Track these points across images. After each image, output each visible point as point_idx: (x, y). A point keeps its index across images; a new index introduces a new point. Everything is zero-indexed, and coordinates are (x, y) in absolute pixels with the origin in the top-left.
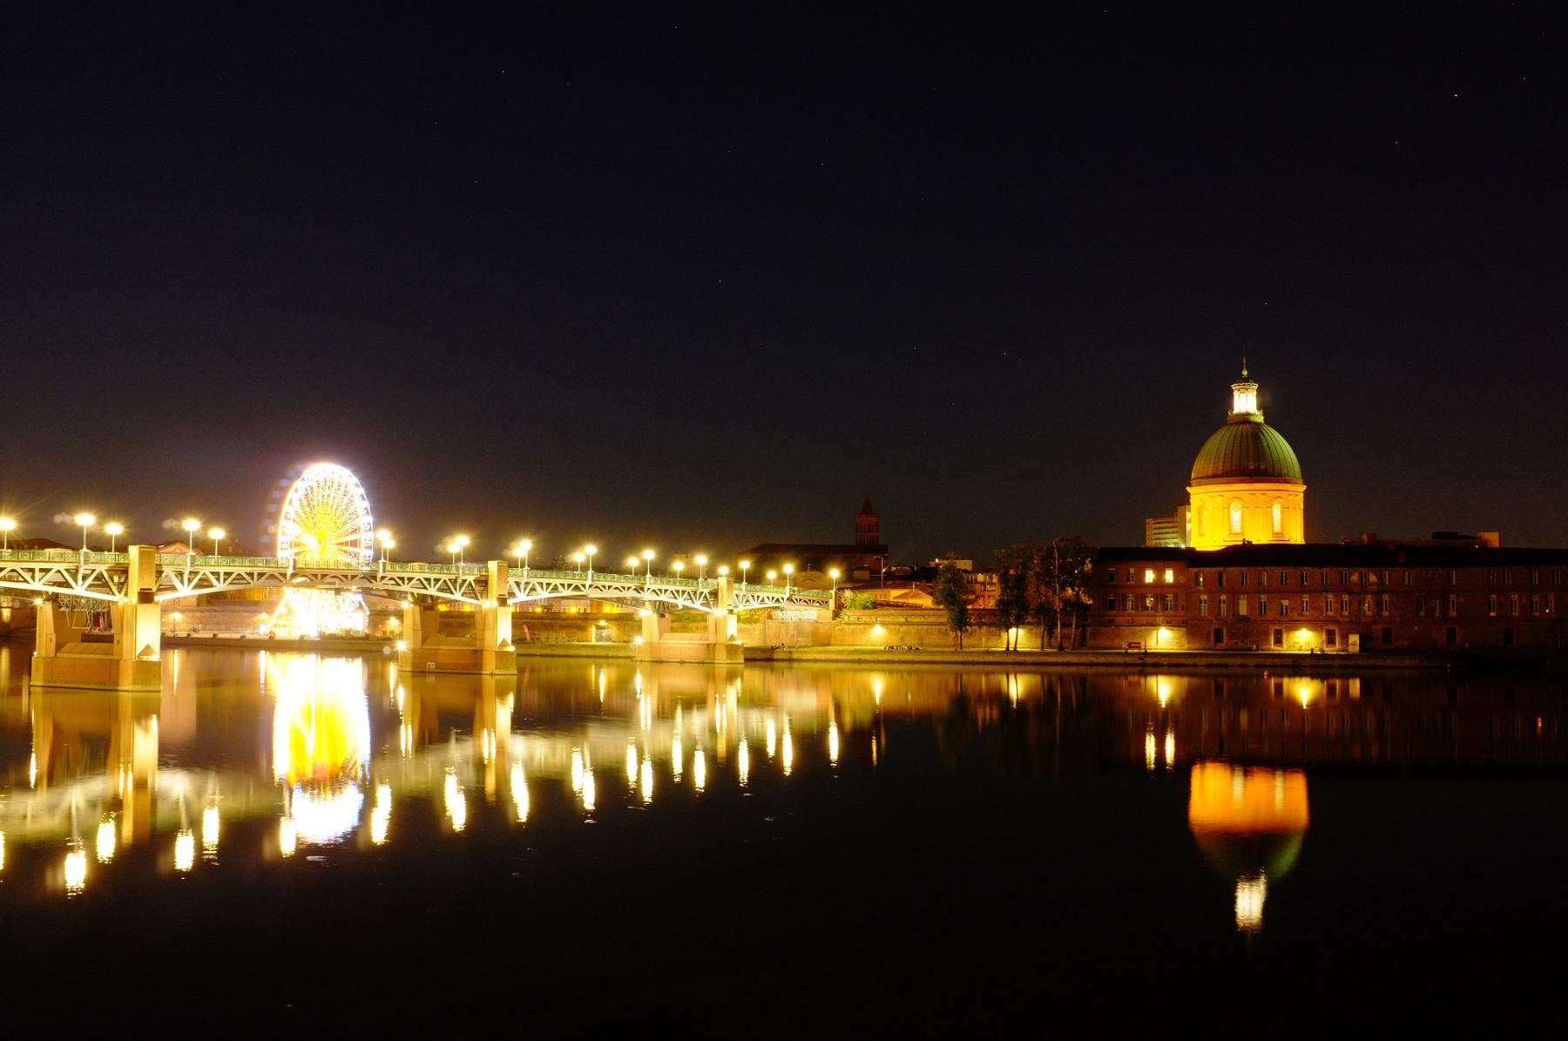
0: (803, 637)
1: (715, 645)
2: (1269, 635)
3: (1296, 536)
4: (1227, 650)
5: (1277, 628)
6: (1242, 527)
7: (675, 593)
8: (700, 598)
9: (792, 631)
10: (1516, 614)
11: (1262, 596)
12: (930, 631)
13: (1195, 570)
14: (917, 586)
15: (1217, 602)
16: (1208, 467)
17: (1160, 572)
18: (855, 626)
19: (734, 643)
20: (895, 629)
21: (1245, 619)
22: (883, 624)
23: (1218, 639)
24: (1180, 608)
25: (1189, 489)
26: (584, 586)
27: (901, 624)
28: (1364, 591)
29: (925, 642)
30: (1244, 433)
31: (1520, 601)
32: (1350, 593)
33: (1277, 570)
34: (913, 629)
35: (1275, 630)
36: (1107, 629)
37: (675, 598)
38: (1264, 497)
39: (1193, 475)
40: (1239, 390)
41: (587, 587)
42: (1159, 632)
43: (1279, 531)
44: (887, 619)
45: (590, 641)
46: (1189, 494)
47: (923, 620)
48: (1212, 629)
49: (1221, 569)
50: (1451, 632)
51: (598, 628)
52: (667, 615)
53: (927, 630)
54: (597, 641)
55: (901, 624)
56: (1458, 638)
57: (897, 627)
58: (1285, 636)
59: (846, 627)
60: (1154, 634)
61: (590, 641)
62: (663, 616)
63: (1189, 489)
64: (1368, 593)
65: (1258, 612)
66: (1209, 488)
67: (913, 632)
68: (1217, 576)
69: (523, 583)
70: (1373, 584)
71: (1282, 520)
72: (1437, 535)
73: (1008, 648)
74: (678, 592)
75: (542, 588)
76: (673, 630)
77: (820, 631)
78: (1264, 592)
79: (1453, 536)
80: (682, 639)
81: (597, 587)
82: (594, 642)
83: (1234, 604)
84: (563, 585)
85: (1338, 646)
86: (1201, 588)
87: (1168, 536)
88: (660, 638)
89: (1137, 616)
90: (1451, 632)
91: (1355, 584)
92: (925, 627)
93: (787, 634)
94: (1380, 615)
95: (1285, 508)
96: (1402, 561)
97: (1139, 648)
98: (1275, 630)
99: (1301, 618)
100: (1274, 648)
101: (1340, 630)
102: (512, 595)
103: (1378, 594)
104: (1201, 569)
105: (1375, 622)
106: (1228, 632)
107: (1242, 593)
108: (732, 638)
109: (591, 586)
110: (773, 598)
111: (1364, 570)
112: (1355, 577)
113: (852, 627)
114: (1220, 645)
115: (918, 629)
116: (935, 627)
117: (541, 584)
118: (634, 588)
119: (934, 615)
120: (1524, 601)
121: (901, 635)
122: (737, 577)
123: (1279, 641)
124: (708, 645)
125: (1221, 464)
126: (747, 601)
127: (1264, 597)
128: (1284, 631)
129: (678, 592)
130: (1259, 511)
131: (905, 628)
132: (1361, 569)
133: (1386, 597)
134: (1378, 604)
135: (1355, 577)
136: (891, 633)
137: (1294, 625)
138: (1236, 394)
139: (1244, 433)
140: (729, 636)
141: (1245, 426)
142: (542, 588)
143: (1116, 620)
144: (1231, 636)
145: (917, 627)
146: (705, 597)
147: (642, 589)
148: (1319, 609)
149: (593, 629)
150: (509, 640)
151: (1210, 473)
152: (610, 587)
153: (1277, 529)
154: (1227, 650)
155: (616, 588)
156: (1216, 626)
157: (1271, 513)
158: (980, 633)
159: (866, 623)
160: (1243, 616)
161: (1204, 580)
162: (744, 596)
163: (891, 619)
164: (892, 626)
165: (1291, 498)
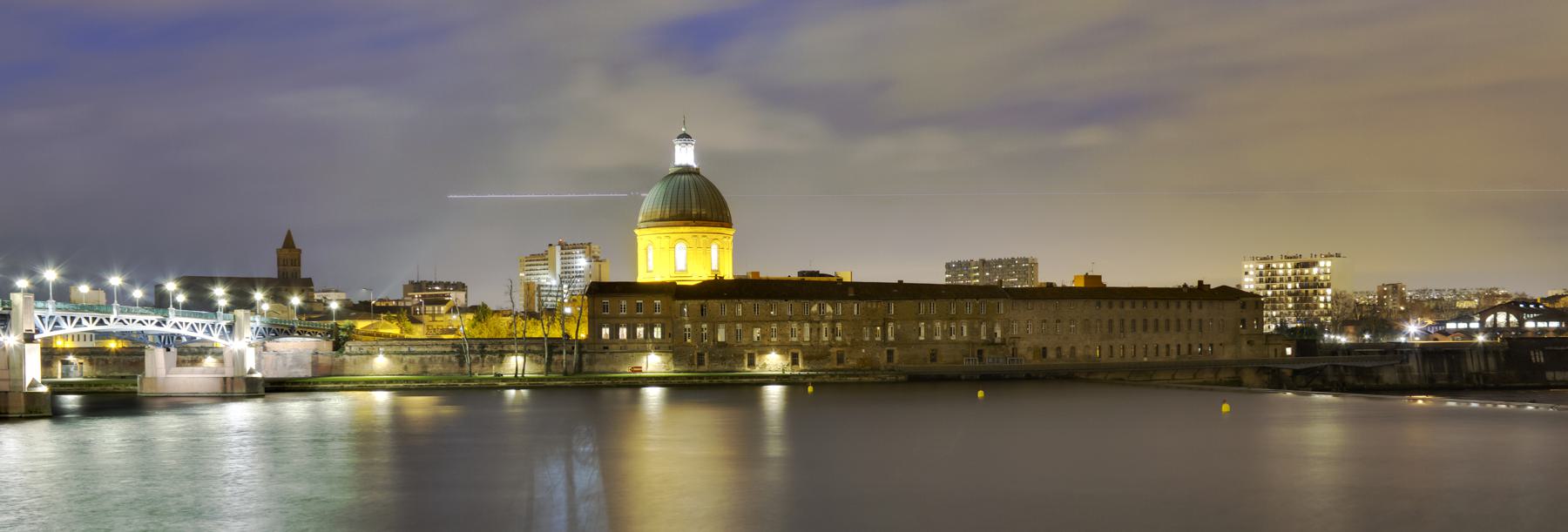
0: (302, 367)
1: (232, 378)
2: (744, 358)
3: (728, 275)
4: (708, 372)
5: (750, 352)
6: (686, 265)
7: (195, 326)
8: (218, 330)
9: (289, 362)
10: (938, 338)
11: (738, 325)
12: (433, 360)
13: (681, 302)
14: (385, 318)
15: (699, 330)
16: (656, 212)
17: (131, 282)
18: (356, 357)
19: (254, 376)
20: (398, 359)
21: (723, 345)
22: (387, 354)
23: (701, 363)
24: (667, 336)
25: (637, 231)
26: (108, 319)
27: (404, 354)
28: (823, 319)
29: (429, 370)
30: (687, 183)
31: (942, 327)
32: (811, 322)
33: (750, 303)
34: (416, 358)
35: (749, 354)
36: (602, 356)
37: (195, 331)
38: (705, 238)
39: (640, 219)
40: (680, 144)
41: (112, 320)
42: (649, 357)
43: (717, 269)
44: (389, 349)
45: (56, 378)
46: (636, 236)
47: (426, 349)
48: (695, 354)
49: (703, 301)
50: (890, 353)
51: (65, 363)
52: (173, 349)
53: (430, 359)
54: (62, 377)
55: (404, 354)
56: (896, 359)
57: (401, 356)
58: (757, 359)
59: (347, 357)
60: (645, 359)
61: (56, 378)
62: (168, 350)
63: (637, 231)
64: (825, 322)
65: (734, 338)
66: (682, 229)
67: (417, 361)
68: (699, 308)
69: (47, 317)
70: (829, 313)
71: (719, 259)
72: (801, 274)
73: (516, 374)
74: (197, 324)
75: (66, 321)
76: (180, 363)
77: (320, 362)
78: (739, 322)
79: (816, 274)
80: (192, 373)
81: (121, 321)
82: (59, 379)
83: (714, 331)
84: (87, 319)
85: (801, 366)
86: (686, 318)
87: (539, 267)
88: (167, 373)
89: (629, 343)
90: (890, 353)
91: (815, 314)
92: (429, 356)
93: (285, 365)
94: (834, 339)
95: (720, 248)
96: (851, 294)
97: (641, 371)
98: (749, 354)
99: (545, 327)
100: (746, 369)
101: (803, 353)
102: (38, 331)
103: (834, 322)
104: (686, 301)
105: (831, 346)
106: (709, 356)
107: (722, 322)
108: (251, 372)
109: (115, 319)
110: (94, 319)
111: (822, 302)
112: (815, 308)
113: (353, 357)
114: (702, 368)
115: (422, 359)
116: (437, 356)
117: (65, 318)
118: (156, 321)
119: (437, 345)
120: (945, 328)
121: (404, 364)
122: (40, 293)
123: (752, 364)
124: (225, 379)
125: (668, 209)
126: (57, 323)
127: (739, 326)
128: (756, 355)
129: (197, 324)
130: (701, 251)
131: (408, 357)
132: (820, 302)
133: (839, 326)
134: (834, 330)
135: (815, 308)
136: (394, 362)
137: (764, 350)
138: (677, 148)
139: (687, 183)
140: (248, 370)
141: (686, 177)
142: (66, 321)
143: (610, 346)
144: (712, 359)
145: (420, 356)
146: (223, 330)
147: (165, 322)
148: (785, 336)
149: (60, 364)
150: (39, 380)
151: (658, 217)
152: (133, 321)
153: (715, 267)
154: (708, 372)
155: (140, 322)
156: (700, 351)
157: (710, 253)
158: (483, 361)
159: (368, 353)
160: (721, 342)
161: (688, 310)
162: (51, 317)
163: (394, 349)
164: (395, 356)
165: (725, 240)
